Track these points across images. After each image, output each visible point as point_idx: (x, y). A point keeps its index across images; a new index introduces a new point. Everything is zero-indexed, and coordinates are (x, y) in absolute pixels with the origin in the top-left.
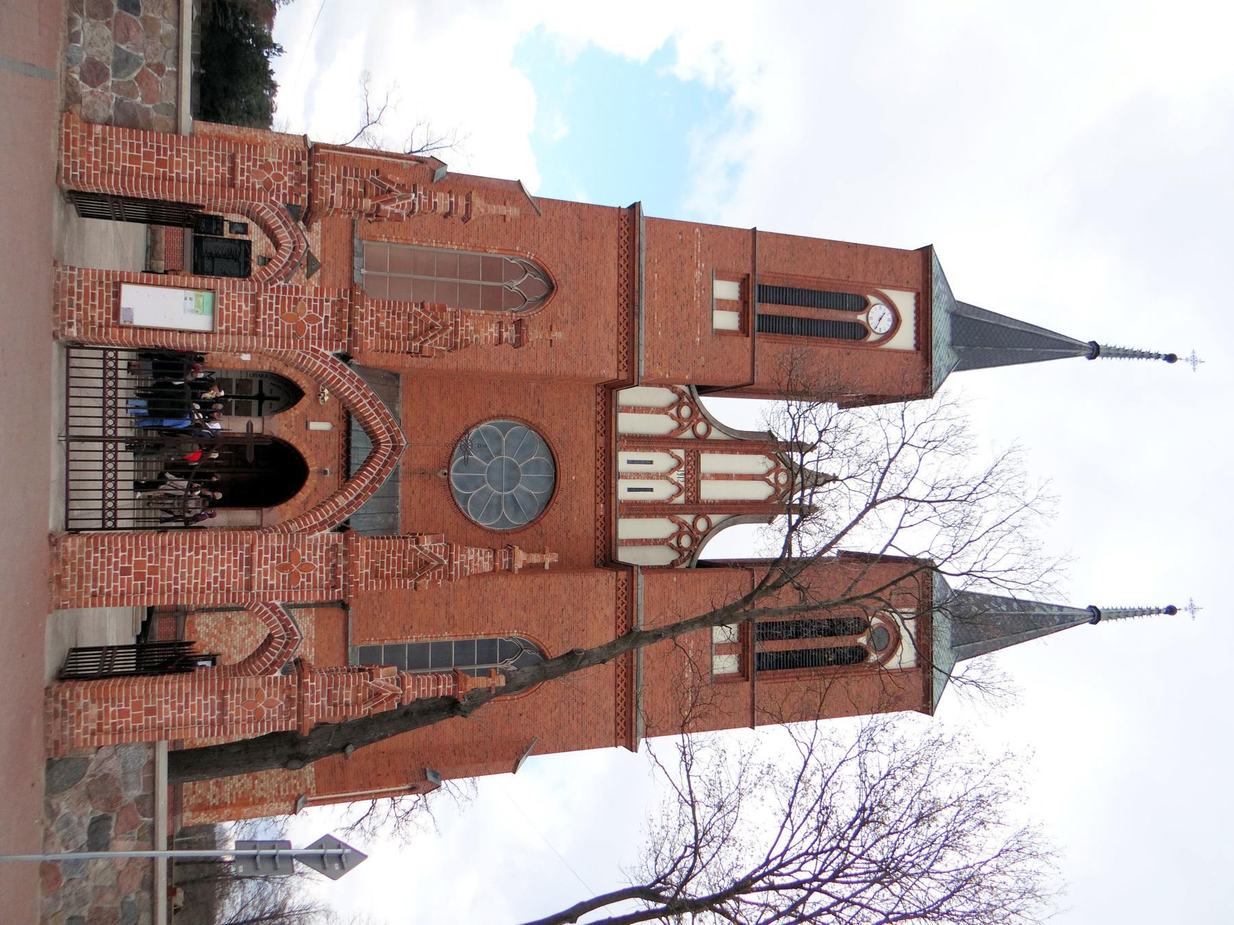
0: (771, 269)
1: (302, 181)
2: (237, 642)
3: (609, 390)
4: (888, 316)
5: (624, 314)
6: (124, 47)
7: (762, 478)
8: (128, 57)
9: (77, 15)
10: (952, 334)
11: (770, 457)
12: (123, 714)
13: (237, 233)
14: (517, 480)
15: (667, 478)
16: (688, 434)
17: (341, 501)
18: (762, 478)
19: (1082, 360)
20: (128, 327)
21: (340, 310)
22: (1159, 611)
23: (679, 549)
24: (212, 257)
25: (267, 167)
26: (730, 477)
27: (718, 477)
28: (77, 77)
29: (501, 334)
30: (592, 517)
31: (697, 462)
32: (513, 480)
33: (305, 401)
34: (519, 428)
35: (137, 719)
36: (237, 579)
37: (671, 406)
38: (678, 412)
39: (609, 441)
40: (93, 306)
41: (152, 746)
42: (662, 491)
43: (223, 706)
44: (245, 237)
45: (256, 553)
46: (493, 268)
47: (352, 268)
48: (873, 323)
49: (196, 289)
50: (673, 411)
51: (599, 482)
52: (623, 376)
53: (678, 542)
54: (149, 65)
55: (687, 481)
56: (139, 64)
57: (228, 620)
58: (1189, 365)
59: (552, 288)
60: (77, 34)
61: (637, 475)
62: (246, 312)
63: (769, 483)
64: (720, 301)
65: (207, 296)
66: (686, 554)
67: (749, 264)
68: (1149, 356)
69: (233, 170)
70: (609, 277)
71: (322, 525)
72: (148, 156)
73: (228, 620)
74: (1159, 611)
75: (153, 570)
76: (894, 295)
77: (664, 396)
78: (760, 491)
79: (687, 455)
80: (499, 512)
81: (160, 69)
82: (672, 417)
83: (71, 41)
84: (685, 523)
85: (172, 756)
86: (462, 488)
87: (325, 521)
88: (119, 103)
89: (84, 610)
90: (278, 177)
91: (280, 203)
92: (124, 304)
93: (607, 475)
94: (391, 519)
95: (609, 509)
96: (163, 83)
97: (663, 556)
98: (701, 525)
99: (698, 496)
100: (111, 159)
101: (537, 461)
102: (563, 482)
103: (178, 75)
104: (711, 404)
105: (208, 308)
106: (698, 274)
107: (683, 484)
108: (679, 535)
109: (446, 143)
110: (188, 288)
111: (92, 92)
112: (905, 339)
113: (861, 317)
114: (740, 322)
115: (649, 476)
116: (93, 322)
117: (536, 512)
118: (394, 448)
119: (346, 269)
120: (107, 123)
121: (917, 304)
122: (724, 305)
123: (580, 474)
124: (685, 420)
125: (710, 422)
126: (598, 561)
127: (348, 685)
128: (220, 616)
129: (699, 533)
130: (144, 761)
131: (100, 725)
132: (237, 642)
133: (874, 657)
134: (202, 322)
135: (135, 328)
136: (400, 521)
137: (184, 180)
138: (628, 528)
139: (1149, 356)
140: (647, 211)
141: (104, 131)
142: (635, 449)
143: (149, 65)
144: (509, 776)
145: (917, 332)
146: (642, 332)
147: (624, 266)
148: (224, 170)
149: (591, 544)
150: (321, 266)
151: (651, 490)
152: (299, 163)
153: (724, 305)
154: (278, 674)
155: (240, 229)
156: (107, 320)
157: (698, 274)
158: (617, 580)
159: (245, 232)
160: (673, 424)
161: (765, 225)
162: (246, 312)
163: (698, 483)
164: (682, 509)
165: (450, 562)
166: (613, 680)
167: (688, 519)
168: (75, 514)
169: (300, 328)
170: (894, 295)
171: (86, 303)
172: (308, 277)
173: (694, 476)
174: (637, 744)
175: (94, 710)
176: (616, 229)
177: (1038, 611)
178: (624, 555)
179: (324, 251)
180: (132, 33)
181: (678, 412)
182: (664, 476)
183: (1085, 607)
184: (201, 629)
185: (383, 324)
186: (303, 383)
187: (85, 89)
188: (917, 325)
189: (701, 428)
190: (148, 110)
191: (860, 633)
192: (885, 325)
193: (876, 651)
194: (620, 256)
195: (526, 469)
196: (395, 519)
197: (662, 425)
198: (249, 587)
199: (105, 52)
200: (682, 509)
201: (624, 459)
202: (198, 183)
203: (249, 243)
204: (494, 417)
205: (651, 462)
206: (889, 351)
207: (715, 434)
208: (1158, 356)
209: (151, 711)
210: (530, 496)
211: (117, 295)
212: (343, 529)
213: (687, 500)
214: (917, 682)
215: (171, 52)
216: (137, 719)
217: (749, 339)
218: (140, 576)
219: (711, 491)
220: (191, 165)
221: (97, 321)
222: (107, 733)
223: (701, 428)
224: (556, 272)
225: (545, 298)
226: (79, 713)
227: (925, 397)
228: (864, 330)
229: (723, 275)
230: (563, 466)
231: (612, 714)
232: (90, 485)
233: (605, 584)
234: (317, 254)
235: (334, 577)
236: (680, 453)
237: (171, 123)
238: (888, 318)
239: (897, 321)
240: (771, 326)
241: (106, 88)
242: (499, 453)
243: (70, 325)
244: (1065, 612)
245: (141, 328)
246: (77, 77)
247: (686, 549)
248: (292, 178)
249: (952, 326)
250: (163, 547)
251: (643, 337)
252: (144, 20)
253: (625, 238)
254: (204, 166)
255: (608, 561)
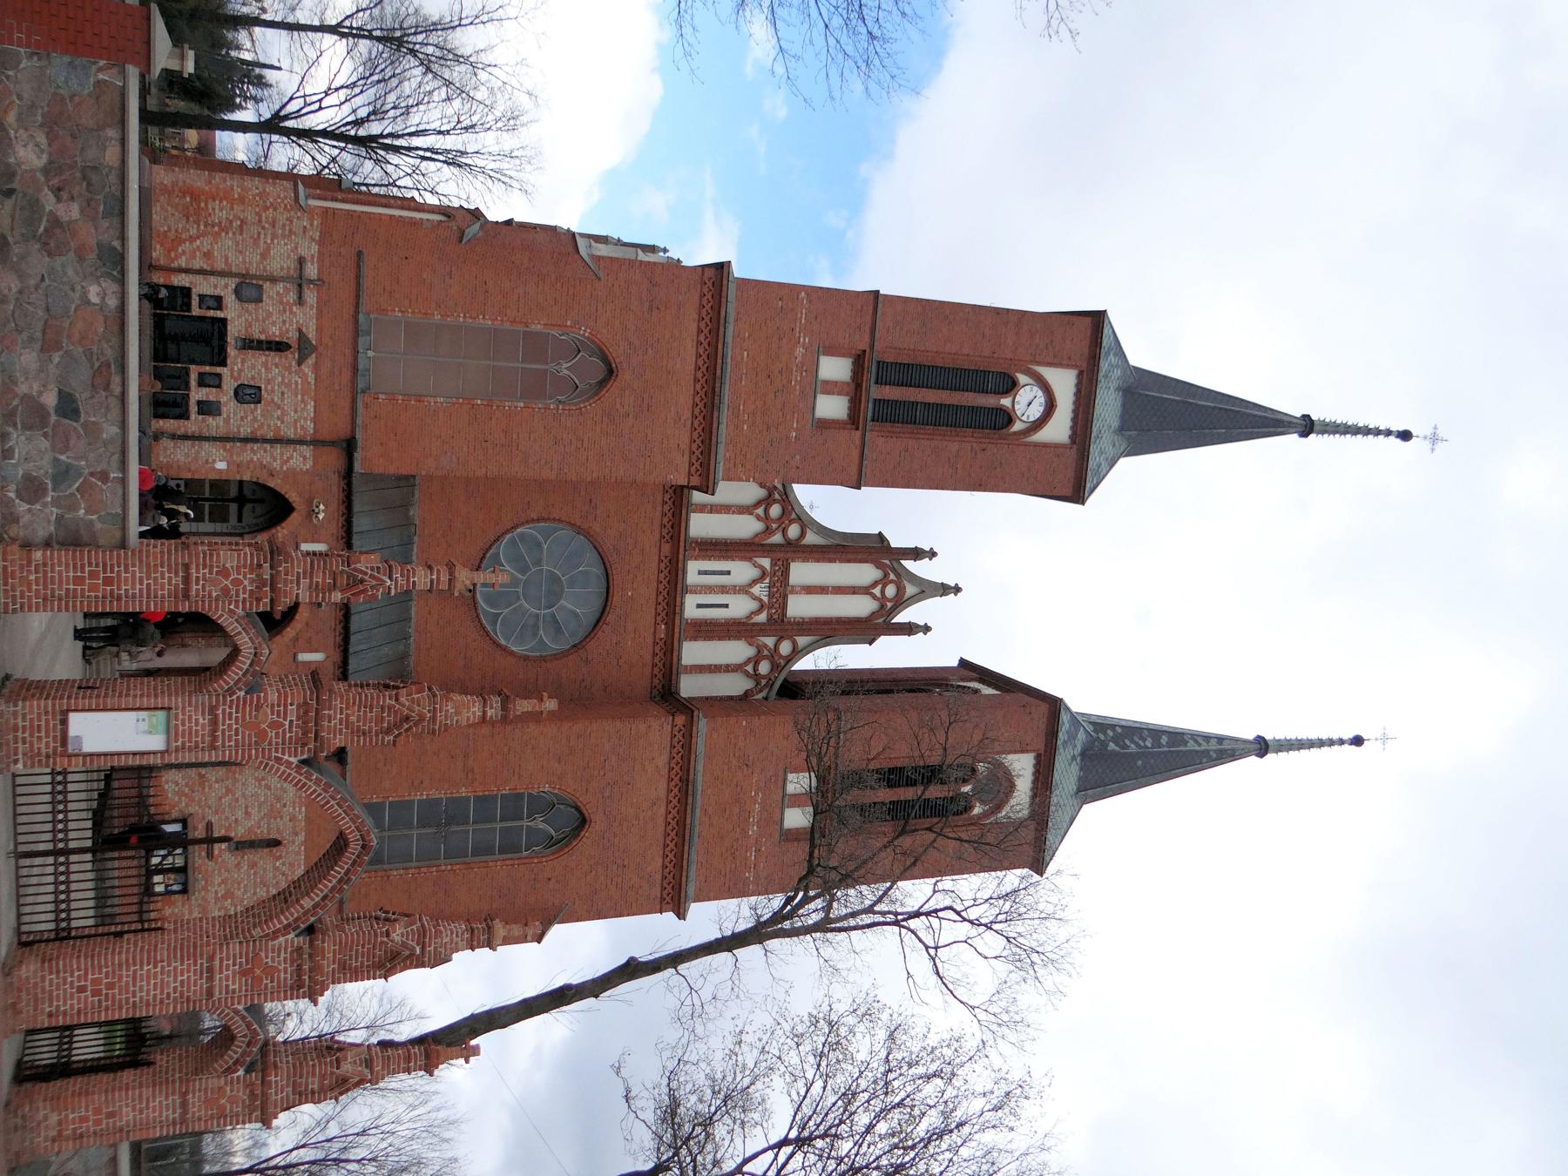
0: (894, 343)
1: (265, 585)
2: (212, 801)
3: (677, 502)
4: (1041, 399)
5: (701, 405)
6: (63, 458)
7: (866, 590)
8: (68, 467)
9: (11, 429)
10: (1122, 417)
11: (879, 566)
12: (84, 1119)
13: (209, 308)
14: (559, 595)
15: (747, 593)
16: (777, 538)
17: (307, 903)
18: (866, 590)
19: (1293, 438)
20: (77, 755)
21: (306, 712)
22: (1341, 742)
23: (756, 676)
24: (177, 339)
25: (224, 573)
26: (820, 591)
27: (810, 590)
28: (12, 495)
29: (485, 713)
30: (650, 640)
31: (786, 572)
32: (554, 595)
33: (294, 518)
34: (564, 533)
35: (98, 1122)
36: (198, 986)
37: (758, 504)
38: (766, 511)
39: (677, 546)
40: (39, 738)
41: (114, 1146)
42: (739, 607)
43: (184, 1105)
44: (219, 314)
45: (217, 962)
46: (536, 346)
47: (356, 352)
48: (1020, 409)
49: (148, 709)
50: (760, 511)
51: (661, 598)
52: (695, 481)
53: (755, 669)
54: (92, 474)
55: (771, 596)
56: (81, 475)
57: (201, 776)
58: (1427, 444)
59: (611, 372)
60: (11, 449)
61: (709, 589)
62: (203, 726)
63: (874, 597)
64: (826, 382)
65: (161, 715)
66: (764, 682)
67: (867, 338)
68: (1377, 432)
69: (187, 580)
70: (685, 358)
71: (287, 929)
72: (93, 575)
73: (201, 776)
74: (1341, 742)
75: (110, 986)
76: (1049, 374)
77: (749, 492)
78: (861, 607)
79: (773, 565)
80: (535, 634)
81: (104, 477)
82: (758, 518)
83: (5, 458)
84: (766, 646)
85: (136, 1148)
86: (491, 605)
87: (289, 925)
88: (59, 519)
89: (20, 615)
90: (237, 582)
91: (240, 611)
92: (72, 732)
93: (673, 587)
94: (401, 647)
95: (672, 626)
96: (108, 494)
97: (735, 685)
98: (785, 648)
99: (784, 614)
100: (53, 583)
101: (586, 573)
102: (616, 599)
103: (124, 482)
104: (807, 495)
105: (162, 727)
106: (800, 351)
107: (765, 599)
108: (756, 661)
109: (512, 12)
110: (140, 709)
111: (29, 510)
112: (1058, 430)
113: (1006, 402)
114: (850, 408)
115: (724, 590)
116: (39, 754)
117: (581, 634)
118: (363, 847)
119: (348, 352)
120: (47, 544)
121: (1079, 386)
122: (831, 388)
123: (638, 591)
124: (773, 521)
125: (806, 522)
126: (655, 692)
127: (314, 1075)
128: (192, 772)
129: (781, 657)
130: (105, 1159)
131: (60, 1131)
132: (212, 801)
133: (977, 810)
134: (156, 742)
135: (85, 756)
136: (413, 646)
137: (134, 596)
138: (693, 652)
139: (1377, 432)
140: (738, 272)
141: (44, 556)
142: (705, 557)
143: (92, 474)
144: (532, 946)
145: (1075, 420)
146: (723, 427)
147: (705, 344)
148: (178, 580)
149: (647, 671)
150: (315, 349)
151: (727, 606)
152: (259, 566)
153: (831, 388)
154: (241, 1072)
155: (212, 303)
156: (55, 749)
157: (800, 351)
158: (673, 726)
159: (220, 307)
160: (758, 526)
161: (890, 287)
162: (203, 726)
163: (785, 597)
164: (762, 629)
165: (423, 949)
166: (661, 840)
167: (770, 641)
168: (27, 909)
169: (262, 735)
170: (1049, 374)
171: (32, 735)
172: (299, 364)
173: (780, 587)
174: (686, 911)
175: (54, 1118)
176: (697, 296)
177: (1192, 746)
178: (689, 687)
179: (319, 329)
180: (72, 442)
181: (766, 511)
182: (744, 590)
183: (1251, 737)
184: (170, 788)
185: (353, 719)
186: (293, 497)
187: (23, 507)
188: (1076, 412)
189: (793, 531)
190: (91, 522)
191: (965, 781)
192: (1036, 412)
193: (983, 802)
194: (700, 331)
195: (572, 583)
196: (407, 646)
197: (745, 527)
198: (210, 993)
199: (42, 467)
200: (762, 629)
201: (694, 570)
202: (148, 597)
203: (224, 321)
204: (533, 520)
205: (728, 573)
206: (1036, 445)
207: (811, 538)
208: (1388, 433)
209: (111, 1115)
210: (576, 615)
211: (64, 722)
212: (311, 930)
213: (770, 618)
214: (1028, 834)
215: (116, 457)
216: (98, 1122)
217: (858, 433)
218: (96, 993)
219: (800, 607)
220: (141, 579)
221: (44, 751)
222: (67, 1139)
223: (793, 531)
224: (617, 353)
225: (602, 384)
226: (39, 1124)
227: (1077, 502)
228: (1008, 417)
229: (832, 351)
230: (617, 580)
231: (658, 877)
232: (42, 889)
233: (657, 730)
234: (312, 335)
235: (299, 976)
236: (766, 562)
237: (118, 534)
238: (1040, 402)
239: (1050, 406)
240: (888, 414)
241: (45, 505)
242: (538, 563)
243: (16, 762)
244: (1226, 746)
245: (91, 755)
246: (12, 495)
247: (764, 677)
248: (252, 581)
249: (1124, 405)
250: (120, 965)
251: (724, 432)
252: (85, 426)
253: (708, 307)
254: (156, 579)
255: (666, 695)
